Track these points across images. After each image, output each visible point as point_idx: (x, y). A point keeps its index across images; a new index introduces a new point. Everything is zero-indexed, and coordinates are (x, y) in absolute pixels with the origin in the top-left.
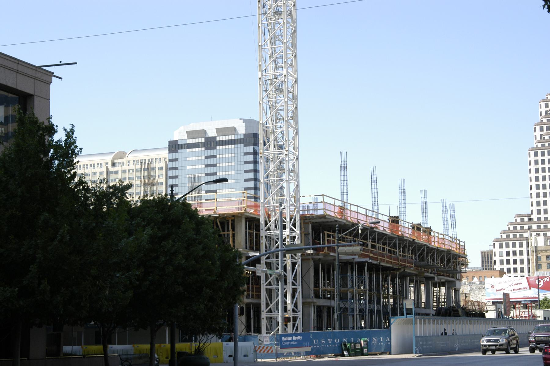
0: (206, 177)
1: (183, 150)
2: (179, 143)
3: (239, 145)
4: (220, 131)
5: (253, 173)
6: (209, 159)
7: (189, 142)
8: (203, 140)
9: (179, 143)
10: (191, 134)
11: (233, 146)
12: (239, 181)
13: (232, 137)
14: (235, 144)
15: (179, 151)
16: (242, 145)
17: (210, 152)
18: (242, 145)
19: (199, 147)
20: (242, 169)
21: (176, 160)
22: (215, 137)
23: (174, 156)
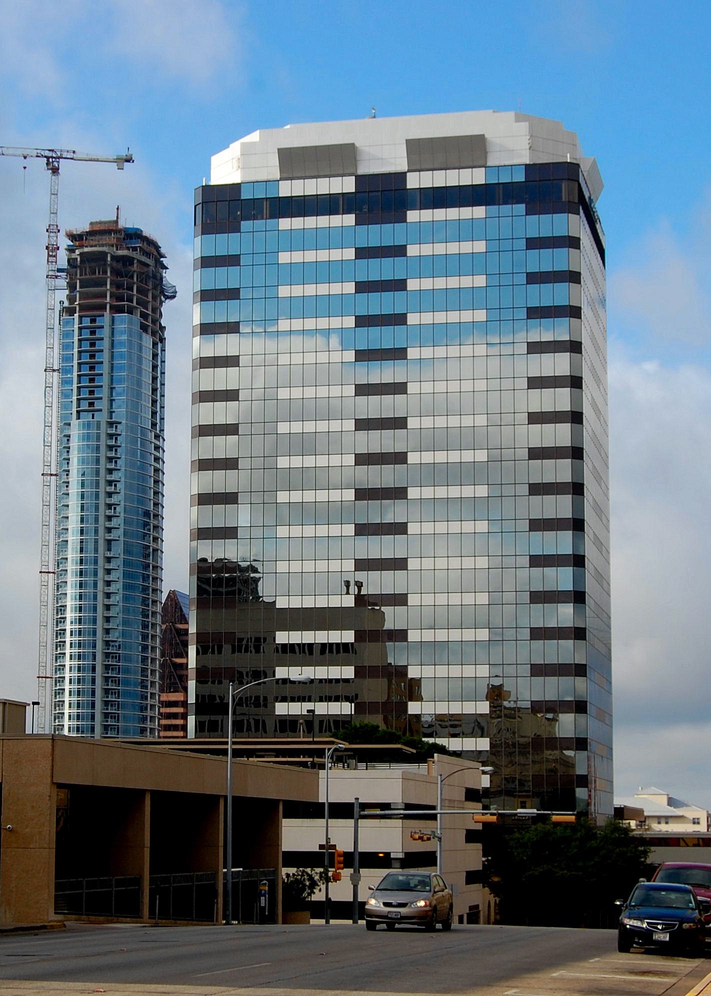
0: (362, 434)
1: (259, 223)
2: (245, 195)
3: (506, 209)
4: (422, 152)
5: (569, 515)
6: (374, 296)
7: (287, 189)
8: (348, 185)
9: (245, 195)
10: (294, 161)
11: (479, 212)
12: (508, 490)
13: (476, 177)
14: (486, 203)
15: (245, 225)
16: (521, 208)
17: (379, 234)
18: (521, 208)
19: (323, 645)
20: (523, 513)
21: (233, 260)
22: (402, 176)
23: (223, 244)
